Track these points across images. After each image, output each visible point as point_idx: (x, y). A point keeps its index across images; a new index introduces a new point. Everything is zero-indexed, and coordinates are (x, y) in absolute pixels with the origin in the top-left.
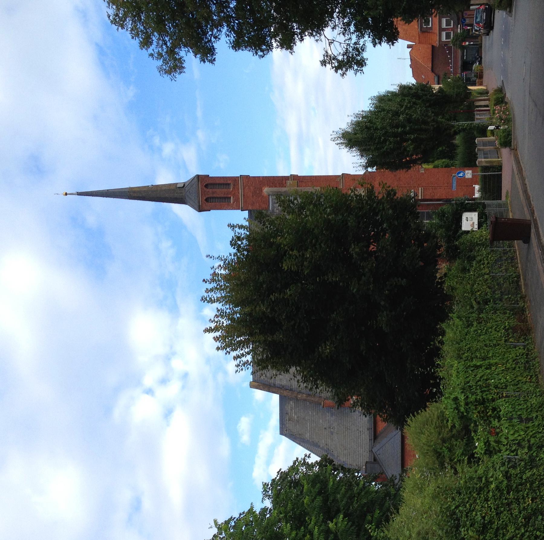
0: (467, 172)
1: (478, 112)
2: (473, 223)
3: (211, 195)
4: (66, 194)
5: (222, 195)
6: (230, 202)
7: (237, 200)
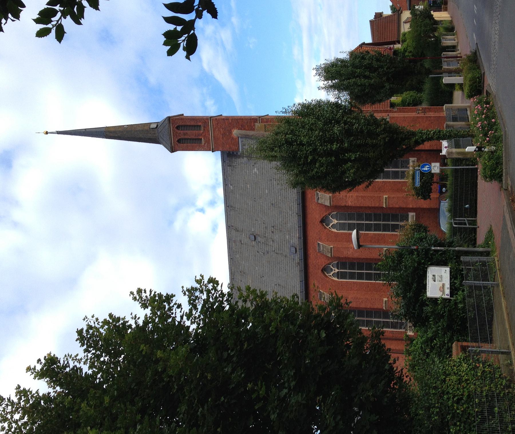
0: (433, 164)
1: (445, 59)
2: (443, 285)
3: (182, 137)
4: (47, 133)
5: (193, 137)
6: (201, 143)
7: (208, 141)
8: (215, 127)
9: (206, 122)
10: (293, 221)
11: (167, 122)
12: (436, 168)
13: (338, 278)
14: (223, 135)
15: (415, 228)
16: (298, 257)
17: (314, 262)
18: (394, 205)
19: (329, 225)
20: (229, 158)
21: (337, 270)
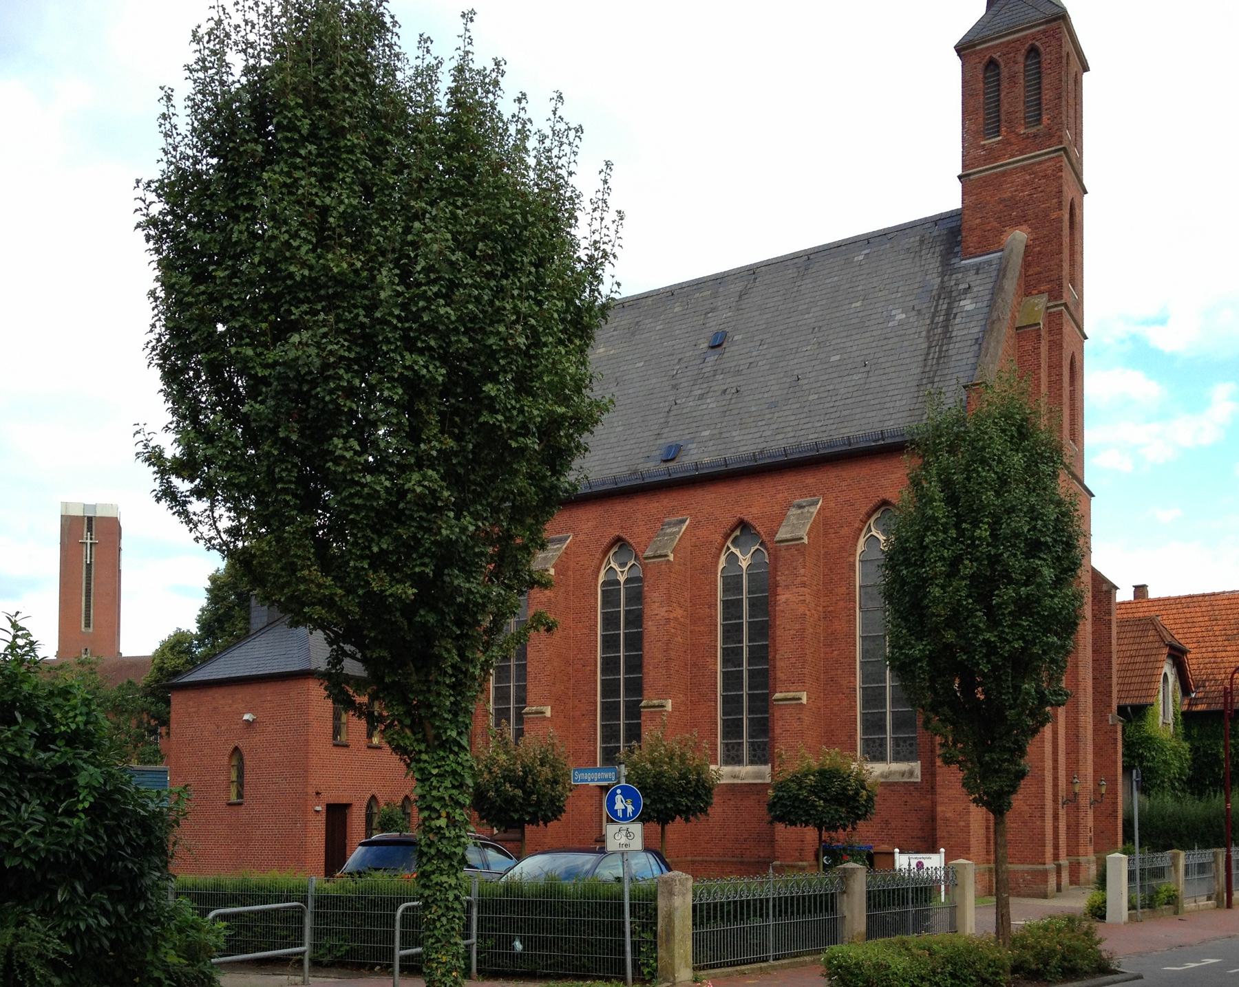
4: (468, 16)
5: (1005, 107)
6: (987, 135)
7: (991, 155)
8: (1037, 168)
9: (1052, 136)
10: (744, 444)
11: (1056, 10)
12: (624, 840)
13: (605, 584)
14: (1012, 198)
15: (689, 782)
16: (653, 468)
17: (639, 515)
18: (780, 723)
19: (735, 547)
20: (947, 236)
21: (622, 579)
